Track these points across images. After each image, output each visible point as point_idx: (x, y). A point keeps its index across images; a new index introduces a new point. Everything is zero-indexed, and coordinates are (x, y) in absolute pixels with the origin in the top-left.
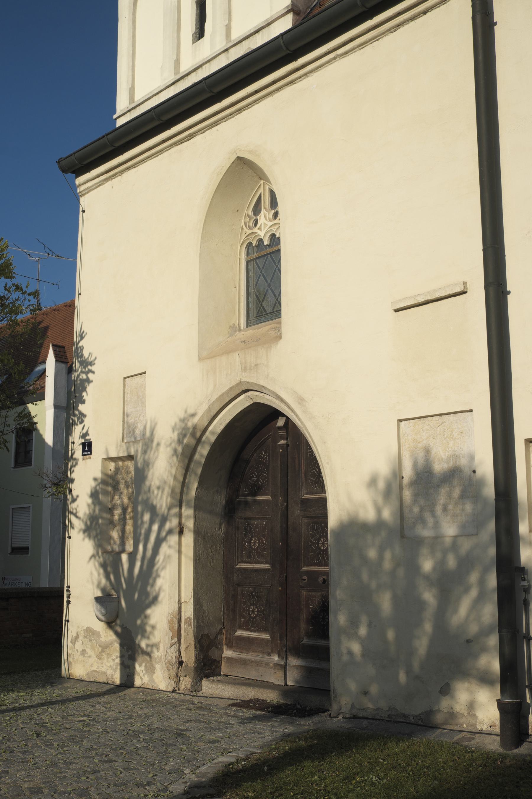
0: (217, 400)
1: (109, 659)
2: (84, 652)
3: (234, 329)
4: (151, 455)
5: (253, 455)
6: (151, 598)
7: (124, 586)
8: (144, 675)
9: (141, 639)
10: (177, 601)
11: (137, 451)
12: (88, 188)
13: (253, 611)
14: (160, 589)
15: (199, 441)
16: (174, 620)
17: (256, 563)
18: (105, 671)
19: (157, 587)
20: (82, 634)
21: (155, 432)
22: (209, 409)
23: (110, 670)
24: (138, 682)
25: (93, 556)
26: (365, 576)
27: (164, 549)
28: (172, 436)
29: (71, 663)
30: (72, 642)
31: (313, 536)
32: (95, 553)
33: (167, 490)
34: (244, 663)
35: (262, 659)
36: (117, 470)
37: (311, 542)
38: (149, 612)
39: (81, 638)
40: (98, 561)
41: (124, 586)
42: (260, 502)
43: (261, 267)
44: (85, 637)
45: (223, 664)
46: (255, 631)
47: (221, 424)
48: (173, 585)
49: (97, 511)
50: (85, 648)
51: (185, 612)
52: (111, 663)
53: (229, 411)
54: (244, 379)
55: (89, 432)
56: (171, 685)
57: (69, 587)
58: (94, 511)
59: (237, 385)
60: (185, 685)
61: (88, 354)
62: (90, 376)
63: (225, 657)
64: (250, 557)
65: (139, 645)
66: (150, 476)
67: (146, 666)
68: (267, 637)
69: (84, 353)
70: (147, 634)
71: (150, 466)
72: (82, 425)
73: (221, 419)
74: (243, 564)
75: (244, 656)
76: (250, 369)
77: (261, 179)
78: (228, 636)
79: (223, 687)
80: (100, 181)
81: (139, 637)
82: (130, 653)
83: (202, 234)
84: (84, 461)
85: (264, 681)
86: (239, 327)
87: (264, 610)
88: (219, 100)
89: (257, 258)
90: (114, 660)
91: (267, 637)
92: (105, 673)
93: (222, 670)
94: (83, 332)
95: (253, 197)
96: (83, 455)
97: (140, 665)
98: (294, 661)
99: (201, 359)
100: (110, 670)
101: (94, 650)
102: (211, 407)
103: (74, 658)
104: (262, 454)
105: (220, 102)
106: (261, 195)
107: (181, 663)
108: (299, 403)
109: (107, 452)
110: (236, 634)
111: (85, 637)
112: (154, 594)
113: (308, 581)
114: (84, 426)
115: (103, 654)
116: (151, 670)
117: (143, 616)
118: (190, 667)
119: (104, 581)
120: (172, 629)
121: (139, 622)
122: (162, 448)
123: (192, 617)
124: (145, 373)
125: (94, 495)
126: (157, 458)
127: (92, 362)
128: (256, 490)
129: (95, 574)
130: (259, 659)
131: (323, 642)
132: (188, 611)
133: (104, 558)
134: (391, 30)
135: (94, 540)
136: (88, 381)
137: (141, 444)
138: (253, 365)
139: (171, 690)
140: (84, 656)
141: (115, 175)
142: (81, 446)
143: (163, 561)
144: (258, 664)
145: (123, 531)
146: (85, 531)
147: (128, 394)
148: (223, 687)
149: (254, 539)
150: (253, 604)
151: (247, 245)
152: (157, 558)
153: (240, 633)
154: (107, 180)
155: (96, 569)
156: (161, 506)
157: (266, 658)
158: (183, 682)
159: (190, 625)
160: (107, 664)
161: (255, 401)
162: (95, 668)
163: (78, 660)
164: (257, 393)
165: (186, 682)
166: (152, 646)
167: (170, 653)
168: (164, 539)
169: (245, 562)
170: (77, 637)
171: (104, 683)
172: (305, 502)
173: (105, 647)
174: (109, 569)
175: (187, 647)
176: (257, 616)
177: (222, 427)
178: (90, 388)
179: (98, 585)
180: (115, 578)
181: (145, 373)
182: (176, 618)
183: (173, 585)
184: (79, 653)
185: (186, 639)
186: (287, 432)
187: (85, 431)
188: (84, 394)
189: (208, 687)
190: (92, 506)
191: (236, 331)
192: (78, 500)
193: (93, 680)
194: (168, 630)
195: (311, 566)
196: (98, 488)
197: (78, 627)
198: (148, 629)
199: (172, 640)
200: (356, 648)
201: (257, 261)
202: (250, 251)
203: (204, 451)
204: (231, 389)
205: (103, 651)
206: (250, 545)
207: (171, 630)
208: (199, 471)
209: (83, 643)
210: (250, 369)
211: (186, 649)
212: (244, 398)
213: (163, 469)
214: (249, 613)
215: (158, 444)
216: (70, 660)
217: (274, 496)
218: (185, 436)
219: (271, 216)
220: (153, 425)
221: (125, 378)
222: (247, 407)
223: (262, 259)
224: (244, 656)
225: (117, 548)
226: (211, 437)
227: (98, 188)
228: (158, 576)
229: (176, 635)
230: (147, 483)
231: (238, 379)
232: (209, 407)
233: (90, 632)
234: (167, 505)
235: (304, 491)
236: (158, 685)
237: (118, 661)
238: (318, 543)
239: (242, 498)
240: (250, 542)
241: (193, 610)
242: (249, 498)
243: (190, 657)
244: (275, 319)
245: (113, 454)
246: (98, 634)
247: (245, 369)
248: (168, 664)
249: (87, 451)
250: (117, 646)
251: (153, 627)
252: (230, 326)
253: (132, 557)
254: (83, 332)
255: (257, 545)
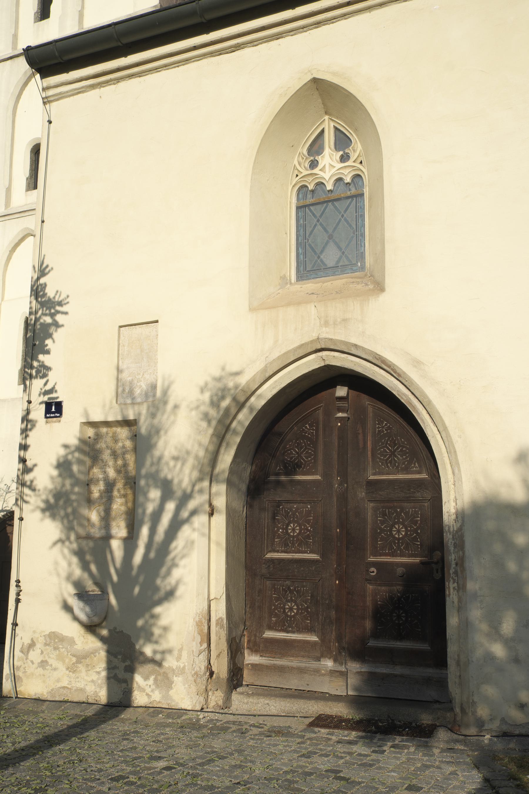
0: (279, 358)
1: (90, 672)
2: (43, 664)
3: (284, 281)
4: (163, 418)
5: (292, 428)
6: (162, 593)
7: (115, 578)
8: (152, 691)
9: (144, 644)
10: (207, 597)
11: (140, 414)
12: (60, 93)
13: (291, 609)
14: (178, 583)
15: (241, 406)
16: (204, 621)
17: (296, 553)
18: (82, 686)
19: (172, 580)
20: (42, 640)
21: (170, 392)
22: (265, 370)
23: (92, 684)
24: (139, 698)
25: (61, 541)
26: (512, 566)
27: (185, 533)
28: (201, 397)
29: (20, 677)
30: (22, 651)
31: (382, 522)
32: (63, 537)
33: (191, 462)
34: (281, 670)
35: (307, 665)
36: (98, 437)
37: (380, 528)
38: (158, 610)
39: (39, 646)
40: (68, 548)
41: (115, 578)
42: (299, 482)
43: (318, 215)
44: (46, 644)
45: (246, 673)
46: (293, 632)
47: (274, 388)
48: (202, 578)
49: (68, 487)
50: (47, 658)
51: (216, 611)
52: (95, 677)
53: (289, 372)
54: (323, 336)
55: (57, 388)
56: (200, 702)
57: (18, 581)
58: (63, 485)
59: (312, 342)
60: (216, 701)
61: (54, 292)
62: (59, 318)
63: (249, 664)
64: (286, 545)
65: (142, 653)
66: (161, 444)
67: (156, 680)
68: (314, 638)
69: (46, 291)
70: (155, 638)
71: (162, 433)
72: (45, 380)
73: (276, 382)
74: (276, 554)
75: (279, 662)
76: (335, 324)
77: (326, 113)
78: (253, 638)
79: (267, 702)
80: (83, 87)
81: (141, 642)
82: (128, 663)
83: (254, 163)
84: (48, 425)
85: (315, 692)
86: (290, 280)
87: (308, 607)
88: (125, 54)
89: (313, 205)
90: (98, 673)
91: (314, 638)
92: (82, 690)
93: (244, 679)
94: (47, 266)
95: (311, 134)
96: (46, 417)
97: (146, 678)
98: (354, 666)
99: (252, 309)
100: (92, 684)
101: (64, 661)
102: (268, 365)
103: (25, 672)
104: (306, 427)
105: (126, 56)
106: (323, 131)
107: (212, 674)
108: (415, 366)
109: (86, 413)
110: (264, 636)
111: (46, 644)
112: (168, 588)
113: (377, 573)
114: (47, 381)
115: (79, 665)
116: (165, 682)
117: (147, 616)
118: (223, 679)
119: (78, 572)
120: (200, 632)
121: (140, 623)
122: (182, 413)
123: (224, 617)
124: (157, 322)
125: (63, 466)
126: (173, 422)
127: (61, 301)
128: (292, 468)
129: (64, 564)
130: (303, 665)
131: (398, 643)
132: (220, 610)
133: (79, 545)
134: (212, 54)
135: (63, 523)
136: (57, 325)
137: (145, 406)
138: (339, 320)
139: (199, 709)
140: (44, 669)
141: (107, 83)
142: (43, 406)
143: (184, 547)
144: (301, 671)
145: (108, 511)
146: (43, 511)
147: (124, 346)
148: (267, 702)
149: (292, 525)
150: (291, 601)
151: (299, 189)
152: (173, 545)
153: (269, 634)
154: (93, 87)
155: (64, 557)
156: (180, 482)
157: (314, 664)
158: (213, 698)
159: (222, 627)
160: (86, 678)
161: (328, 363)
162: (65, 683)
163: (32, 674)
164: (336, 354)
165: (216, 698)
166: (163, 652)
167: (197, 663)
168: (187, 521)
169: (278, 551)
170: (32, 645)
171: (84, 703)
172: (371, 484)
173: (82, 658)
174: (88, 557)
175: (219, 655)
176: (296, 614)
177: (275, 391)
178: (58, 335)
179: (69, 578)
180: (98, 569)
181: (157, 322)
182: (205, 619)
183: (202, 578)
184: (36, 665)
185: (217, 644)
186: (348, 404)
187: (48, 387)
188: (48, 342)
189: (241, 702)
190: (59, 480)
191: (287, 284)
192: (36, 469)
193: (61, 699)
194: (196, 634)
195: (380, 556)
196: (70, 457)
197: (34, 632)
198: (157, 631)
199: (201, 646)
200: (498, 650)
201: (312, 208)
202: (300, 196)
203: (245, 418)
204: (301, 346)
205: (79, 662)
206: (287, 532)
207: (199, 634)
208: (238, 439)
209: (42, 652)
210: (335, 324)
211: (218, 656)
212: (314, 359)
213: (182, 438)
214: (284, 611)
215: (176, 407)
216: (19, 673)
217: (325, 475)
218: (223, 398)
219: (307, 165)
220: (166, 384)
221: (121, 327)
222: (313, 370)
223: (318, 207)
224: (279, 662)
225: (97, 532)
226: (258, 402)
227: (75, 97)
228: (174, 565)
229: (206, 640)
230: (157, 453)
231: (314, 336)
232: (266, 366)
233: (55, 639)
234: (190, 480)
235: (370, 471)
236: (178, 703)
237: (104, 674)
238: (391, 531)
239: (272, 478)
240: (287, 529)
241: (225, 608)
242: (283, 478)
243: (221, 667)
244: (339, 275)
245: (97, 417)
246: (72, 641)
247: (326, 324)
248: (195, 676)
249: (53, 413)
250: (103, 654)
251: (166, 629)
252: (281, 277)
253: (130, 542)
254: (47, 266)
255: (298, 531)
